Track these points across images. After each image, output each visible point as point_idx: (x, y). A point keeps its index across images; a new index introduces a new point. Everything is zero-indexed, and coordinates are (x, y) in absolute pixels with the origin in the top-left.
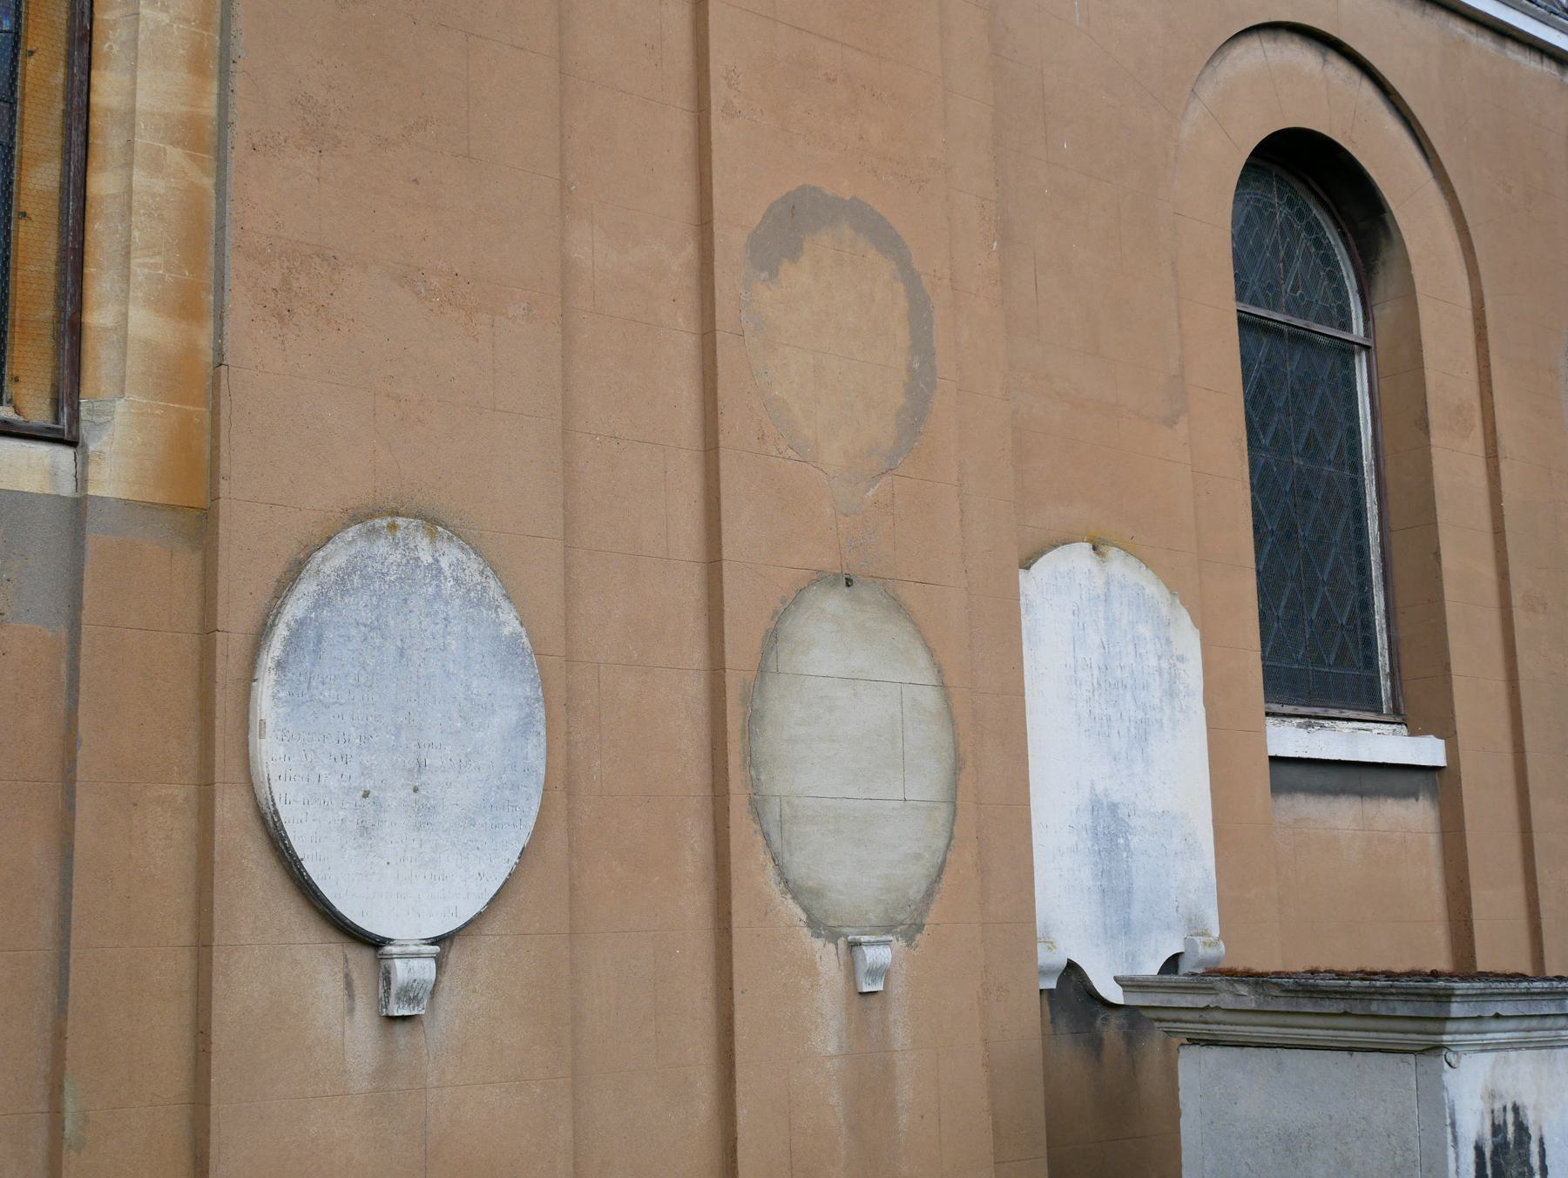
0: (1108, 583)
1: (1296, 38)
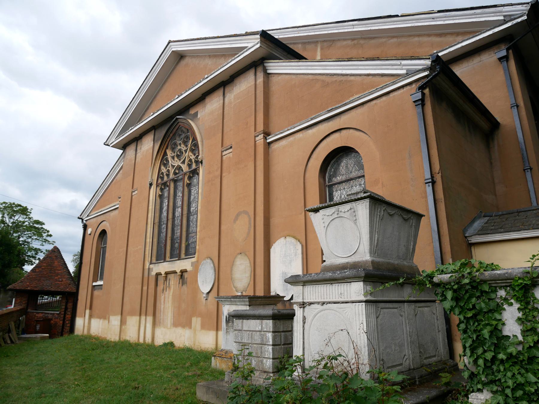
0: (286, 242)
1: (334, 134)
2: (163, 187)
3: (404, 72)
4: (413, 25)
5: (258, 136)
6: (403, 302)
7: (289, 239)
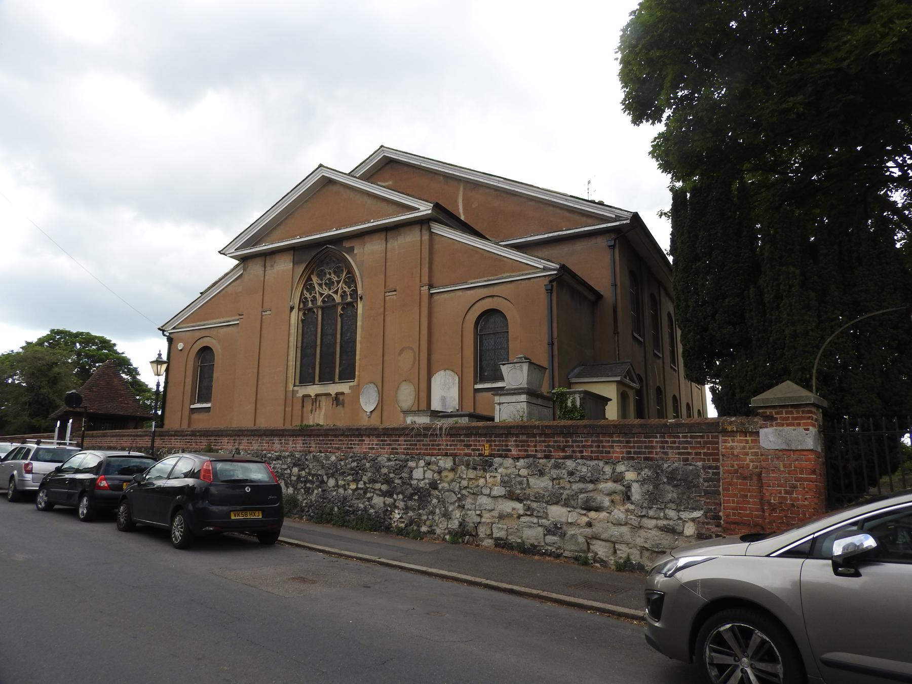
2: (307, 312)
3: (542, 267)
4: (550, 199)
5: (423, 287)
6: (538, 405)
7: (448, 372)
